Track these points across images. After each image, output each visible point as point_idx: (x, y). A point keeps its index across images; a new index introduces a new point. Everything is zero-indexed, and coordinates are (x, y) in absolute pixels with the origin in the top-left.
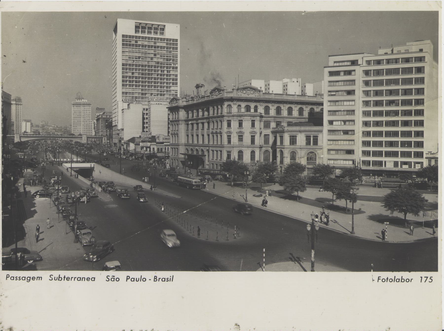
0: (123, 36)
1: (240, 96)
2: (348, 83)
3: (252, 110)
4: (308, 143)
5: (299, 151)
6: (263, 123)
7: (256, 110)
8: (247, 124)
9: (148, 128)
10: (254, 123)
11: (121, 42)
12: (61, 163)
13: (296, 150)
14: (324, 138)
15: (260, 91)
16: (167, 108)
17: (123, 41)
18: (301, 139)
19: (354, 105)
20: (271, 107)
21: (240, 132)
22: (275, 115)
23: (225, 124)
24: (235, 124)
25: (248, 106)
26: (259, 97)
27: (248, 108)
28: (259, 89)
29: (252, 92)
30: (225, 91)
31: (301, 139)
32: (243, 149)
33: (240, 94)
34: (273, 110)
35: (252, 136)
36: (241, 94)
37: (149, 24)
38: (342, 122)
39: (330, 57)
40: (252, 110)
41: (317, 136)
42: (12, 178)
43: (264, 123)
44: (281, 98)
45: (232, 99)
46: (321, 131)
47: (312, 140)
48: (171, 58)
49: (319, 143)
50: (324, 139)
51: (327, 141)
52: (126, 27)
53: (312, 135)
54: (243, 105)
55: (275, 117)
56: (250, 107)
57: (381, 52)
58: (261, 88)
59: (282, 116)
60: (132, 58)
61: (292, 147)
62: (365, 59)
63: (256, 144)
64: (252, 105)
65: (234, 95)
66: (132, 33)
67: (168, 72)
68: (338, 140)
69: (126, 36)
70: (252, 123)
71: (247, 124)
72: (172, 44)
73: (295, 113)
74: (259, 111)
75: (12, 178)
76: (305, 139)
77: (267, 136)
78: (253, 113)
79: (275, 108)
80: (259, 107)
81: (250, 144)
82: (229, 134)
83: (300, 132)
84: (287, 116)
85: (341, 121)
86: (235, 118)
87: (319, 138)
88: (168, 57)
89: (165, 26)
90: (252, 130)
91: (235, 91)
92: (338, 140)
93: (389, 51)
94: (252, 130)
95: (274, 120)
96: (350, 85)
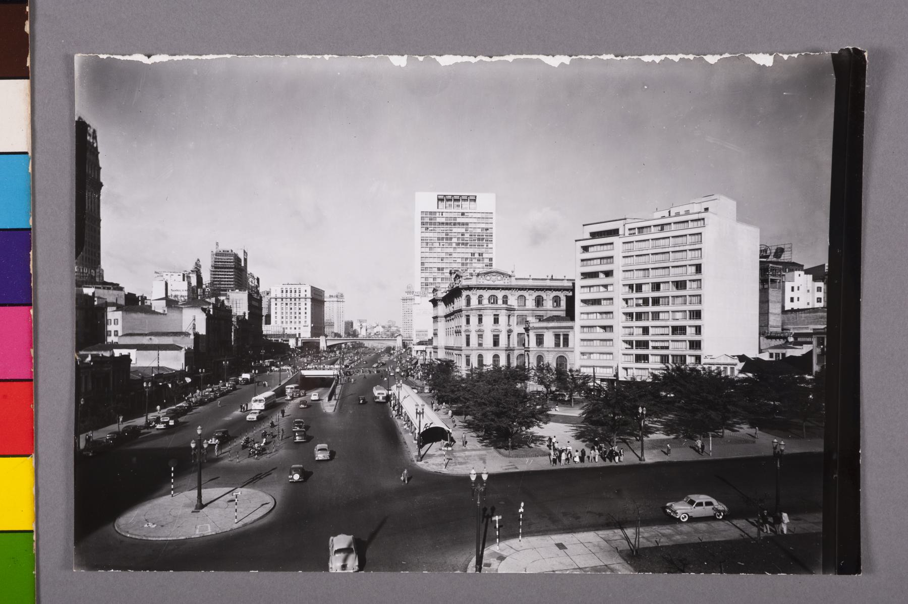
3: (500, 302)
4: (557, 345)
5: (546, 353)
7: (505, 301)
9: (690, 334)
11: (420, 221)
14: (576, 337)
18: (549, 339)
21: (479, 331)
31: (549, 339)
40: (500, 302)
42: (170, 386)
45: (469, 288)
47: (563, 340)
53: (561, 332)
54: (486, 294)
64: (500, 294)
65: (473, 282)
68: (592, 340)
73: (548, 304)
75: (170, 386)
76: (553, 338)
80: (510, 297)
83: (547, 328)
84: (534, 307)
90: (495, 327)
91: (474, 278)
92: (592, 340)
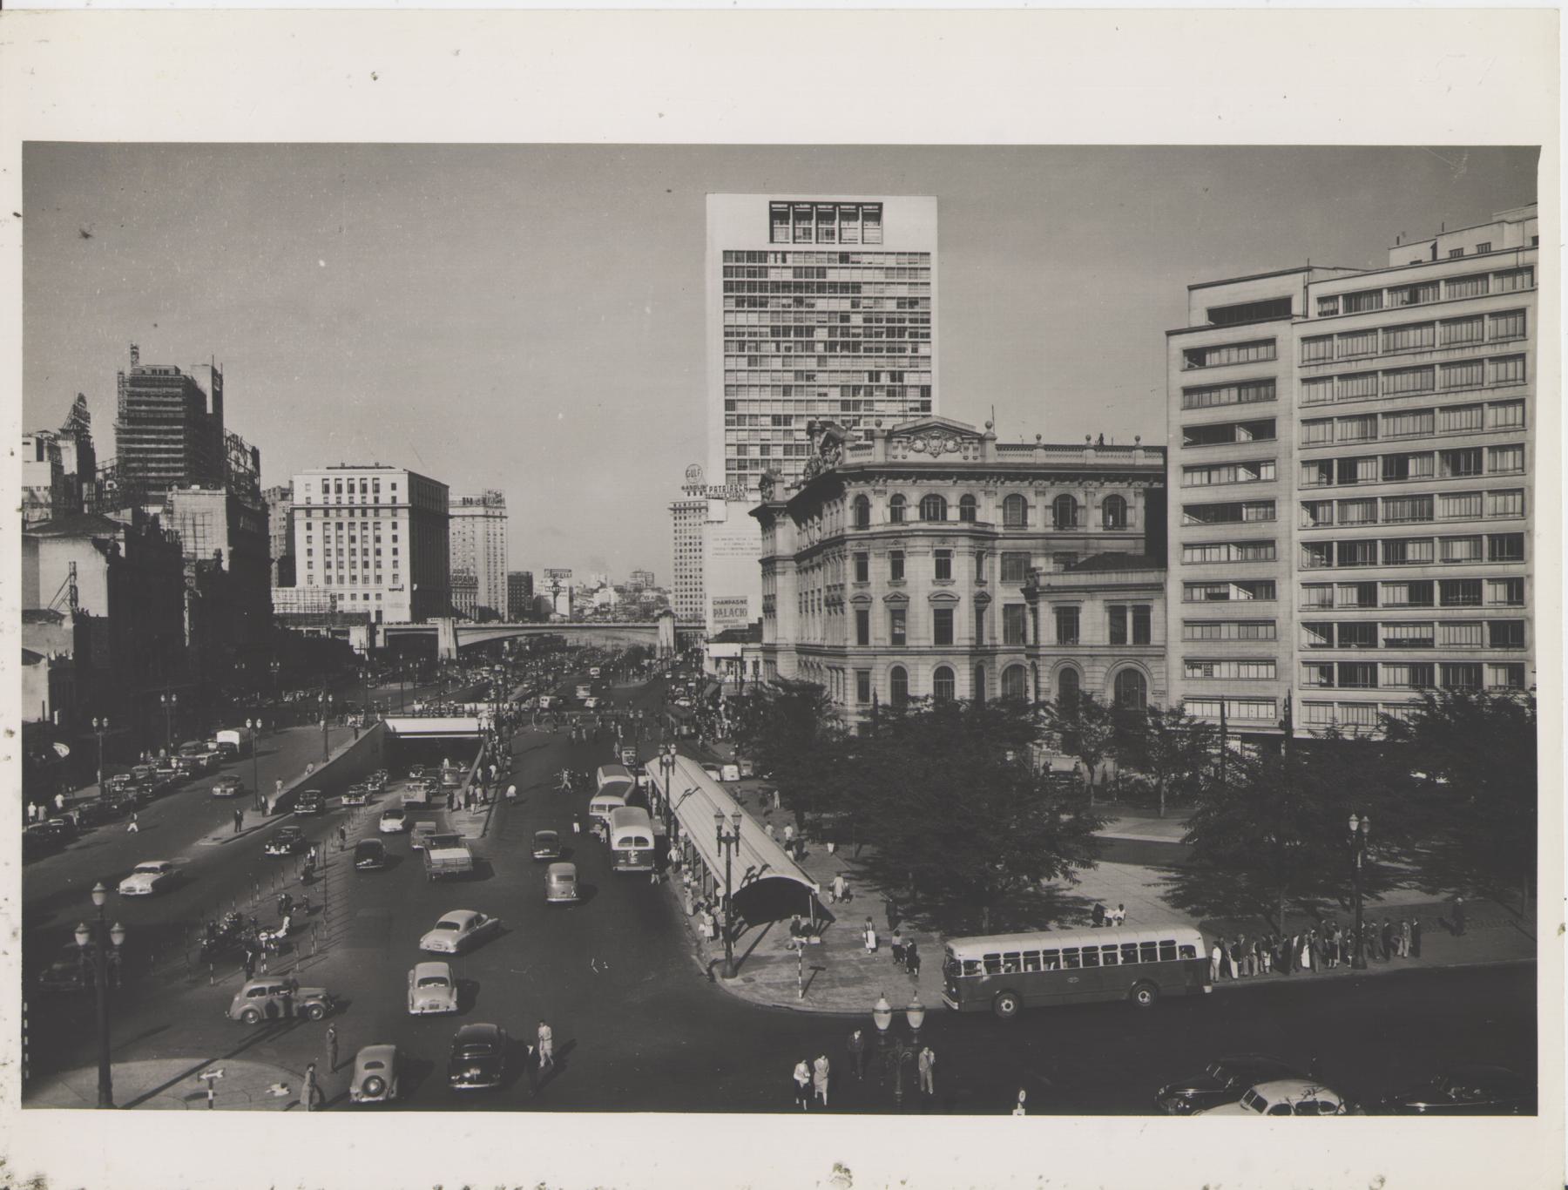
0: (727, 254)
1: (900, 459)
2: (1252, 392)
3: (953, 514)
4: (1117, 637)
6: (998, 560)
8: (920, 569)
10: (948, 564)
12: (1205, 747)
13: (1078, 664)
14: (1172, 613)
15: (982, 439)
16: (752, 513)
17: (725, 275)
18: (1093, 622)
19: (1275, 480)
20: (1031, 498)
22: (1051, 530)
23: (850, 567)
24: (879, 569)
25: (936, 496)
26: (979, 461)
27: (933, 507)
28: (981, 430)
29: (950, 444)
30: (849, 445)
31: (1093, 622)
32: (907, 661)
33: (899, 452)
34: (1040, 508)
35: (937, 613)
36: (906, 452)
37: (822, 197)
38: (1233, 549)
39: (1195, 292)
40: (953, 514)
41: (1077, 610)
43: (1003, 562)
44: (1125, 461)
45: (865, 474)
46: (1159, 588)
47: (1130, 624)
48: (907, 324)
49: (1156, 636)
50: (1171, 616)
51: (1180, 626)
52: (737, 220)
55: (1046, 537)
56: (944, 501)
57: (1400, 256)
58: (988, 426)
59: (1080, 530)
60: (738, 334)
61: (1063, 651)
62: (1316, 291)
63: (955, 642)
64: (953, 495)
66: (760, 242)
67: (893, 379)
69: (739, 255)
70: (938, 564)
71: (920, 569)
72: (912, 264)
74: (980, 516)
77: (1018, 613)
78: (955, 523)
79: (1050, 503)
80: (982, 499)
81: (932, 642)
82: (862, 606)
85: (1228, 544)
86: (879, 542)
87: (1156, 615)
88: (893, 321)
89: (880, 205)
90: (938, 588)
91: (879, 445)
93: (1423, 252)
94: (938, 588)
95: (1046, 548)
96: (1257, 400)
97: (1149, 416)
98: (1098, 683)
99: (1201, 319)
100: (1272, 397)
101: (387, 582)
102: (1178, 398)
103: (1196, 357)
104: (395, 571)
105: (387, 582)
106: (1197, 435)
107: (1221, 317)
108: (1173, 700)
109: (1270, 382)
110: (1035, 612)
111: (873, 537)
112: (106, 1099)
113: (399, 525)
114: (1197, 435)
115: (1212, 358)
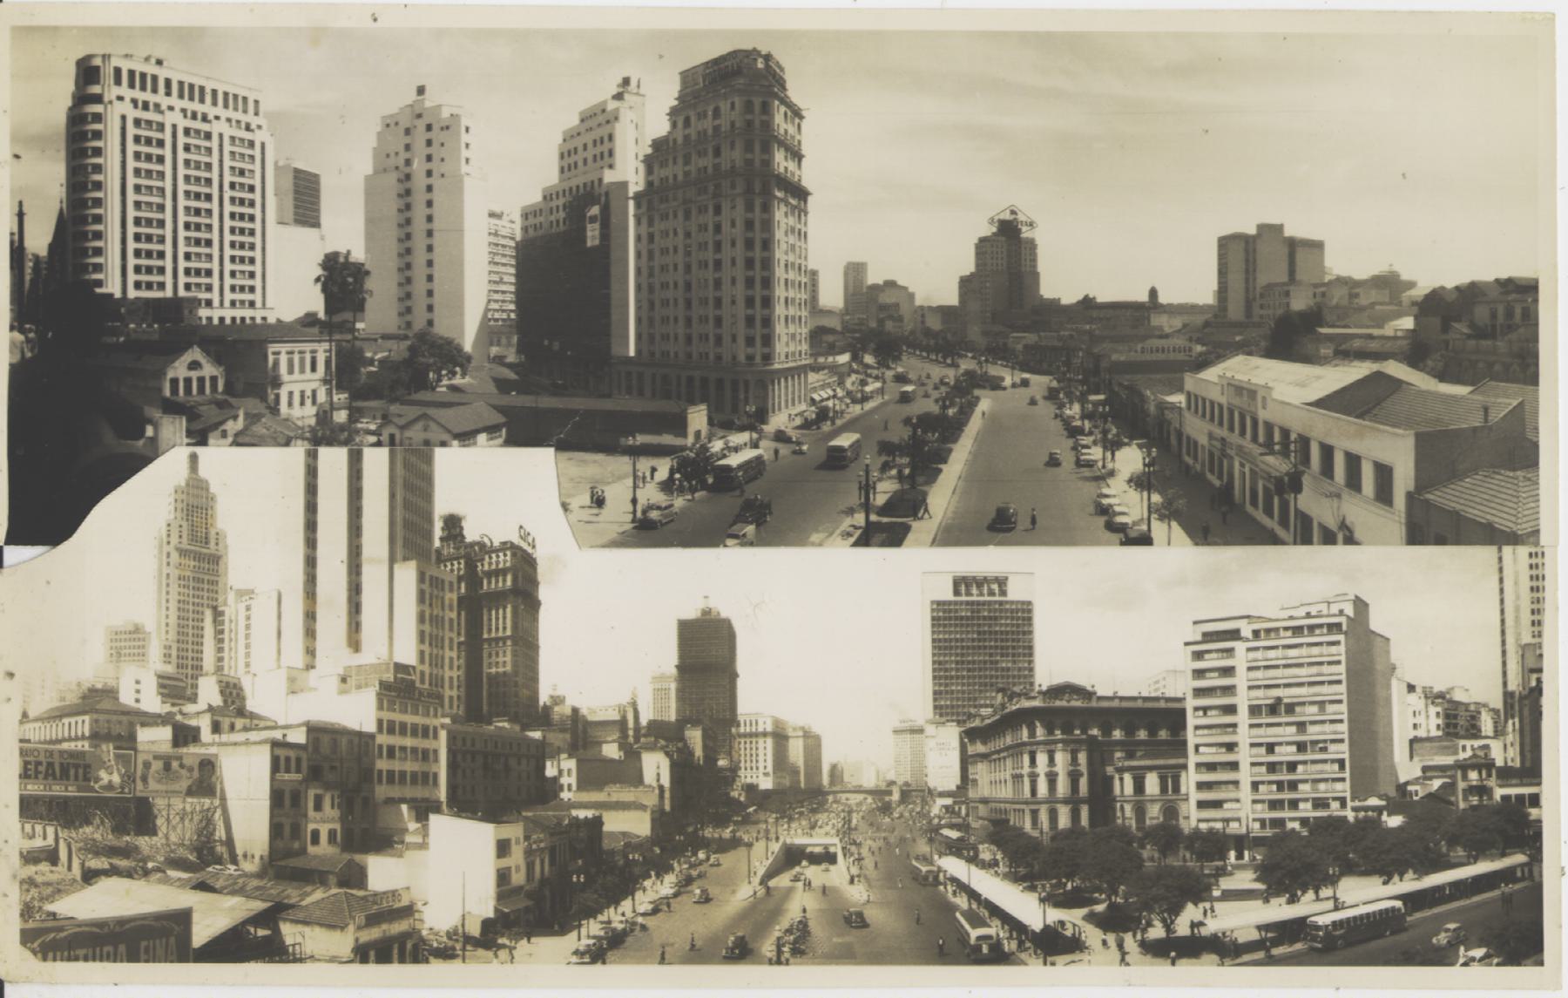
4: (1164, 789)
14: (1190, 780)
18: (1152, 783)
23: (1026, 758)
31: (1152, 783)
46: (1185, 767)
47: (1170, 780)
49: (1183, 790)
97: (1180, 686)
98: (1154, 812)
99: (1199, 638)
100: (1235, 733)
101: (761, 770)
102: (1190, 674)
103: (1198, 656)
104: (429, 226)
105: (761, 770)
106: (1198, 692)
107: (1208, 637)
108: (1193, 823)
109: (1233, 668)
110: (1121, 779)
111: (1039, 743)
112: (69, 959)
113: (424, 143)
114: (1198, 692)
115: (1207, 656)
